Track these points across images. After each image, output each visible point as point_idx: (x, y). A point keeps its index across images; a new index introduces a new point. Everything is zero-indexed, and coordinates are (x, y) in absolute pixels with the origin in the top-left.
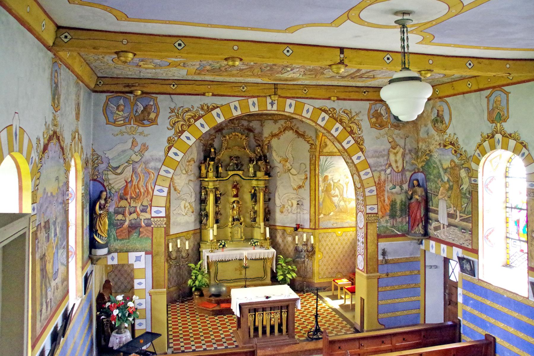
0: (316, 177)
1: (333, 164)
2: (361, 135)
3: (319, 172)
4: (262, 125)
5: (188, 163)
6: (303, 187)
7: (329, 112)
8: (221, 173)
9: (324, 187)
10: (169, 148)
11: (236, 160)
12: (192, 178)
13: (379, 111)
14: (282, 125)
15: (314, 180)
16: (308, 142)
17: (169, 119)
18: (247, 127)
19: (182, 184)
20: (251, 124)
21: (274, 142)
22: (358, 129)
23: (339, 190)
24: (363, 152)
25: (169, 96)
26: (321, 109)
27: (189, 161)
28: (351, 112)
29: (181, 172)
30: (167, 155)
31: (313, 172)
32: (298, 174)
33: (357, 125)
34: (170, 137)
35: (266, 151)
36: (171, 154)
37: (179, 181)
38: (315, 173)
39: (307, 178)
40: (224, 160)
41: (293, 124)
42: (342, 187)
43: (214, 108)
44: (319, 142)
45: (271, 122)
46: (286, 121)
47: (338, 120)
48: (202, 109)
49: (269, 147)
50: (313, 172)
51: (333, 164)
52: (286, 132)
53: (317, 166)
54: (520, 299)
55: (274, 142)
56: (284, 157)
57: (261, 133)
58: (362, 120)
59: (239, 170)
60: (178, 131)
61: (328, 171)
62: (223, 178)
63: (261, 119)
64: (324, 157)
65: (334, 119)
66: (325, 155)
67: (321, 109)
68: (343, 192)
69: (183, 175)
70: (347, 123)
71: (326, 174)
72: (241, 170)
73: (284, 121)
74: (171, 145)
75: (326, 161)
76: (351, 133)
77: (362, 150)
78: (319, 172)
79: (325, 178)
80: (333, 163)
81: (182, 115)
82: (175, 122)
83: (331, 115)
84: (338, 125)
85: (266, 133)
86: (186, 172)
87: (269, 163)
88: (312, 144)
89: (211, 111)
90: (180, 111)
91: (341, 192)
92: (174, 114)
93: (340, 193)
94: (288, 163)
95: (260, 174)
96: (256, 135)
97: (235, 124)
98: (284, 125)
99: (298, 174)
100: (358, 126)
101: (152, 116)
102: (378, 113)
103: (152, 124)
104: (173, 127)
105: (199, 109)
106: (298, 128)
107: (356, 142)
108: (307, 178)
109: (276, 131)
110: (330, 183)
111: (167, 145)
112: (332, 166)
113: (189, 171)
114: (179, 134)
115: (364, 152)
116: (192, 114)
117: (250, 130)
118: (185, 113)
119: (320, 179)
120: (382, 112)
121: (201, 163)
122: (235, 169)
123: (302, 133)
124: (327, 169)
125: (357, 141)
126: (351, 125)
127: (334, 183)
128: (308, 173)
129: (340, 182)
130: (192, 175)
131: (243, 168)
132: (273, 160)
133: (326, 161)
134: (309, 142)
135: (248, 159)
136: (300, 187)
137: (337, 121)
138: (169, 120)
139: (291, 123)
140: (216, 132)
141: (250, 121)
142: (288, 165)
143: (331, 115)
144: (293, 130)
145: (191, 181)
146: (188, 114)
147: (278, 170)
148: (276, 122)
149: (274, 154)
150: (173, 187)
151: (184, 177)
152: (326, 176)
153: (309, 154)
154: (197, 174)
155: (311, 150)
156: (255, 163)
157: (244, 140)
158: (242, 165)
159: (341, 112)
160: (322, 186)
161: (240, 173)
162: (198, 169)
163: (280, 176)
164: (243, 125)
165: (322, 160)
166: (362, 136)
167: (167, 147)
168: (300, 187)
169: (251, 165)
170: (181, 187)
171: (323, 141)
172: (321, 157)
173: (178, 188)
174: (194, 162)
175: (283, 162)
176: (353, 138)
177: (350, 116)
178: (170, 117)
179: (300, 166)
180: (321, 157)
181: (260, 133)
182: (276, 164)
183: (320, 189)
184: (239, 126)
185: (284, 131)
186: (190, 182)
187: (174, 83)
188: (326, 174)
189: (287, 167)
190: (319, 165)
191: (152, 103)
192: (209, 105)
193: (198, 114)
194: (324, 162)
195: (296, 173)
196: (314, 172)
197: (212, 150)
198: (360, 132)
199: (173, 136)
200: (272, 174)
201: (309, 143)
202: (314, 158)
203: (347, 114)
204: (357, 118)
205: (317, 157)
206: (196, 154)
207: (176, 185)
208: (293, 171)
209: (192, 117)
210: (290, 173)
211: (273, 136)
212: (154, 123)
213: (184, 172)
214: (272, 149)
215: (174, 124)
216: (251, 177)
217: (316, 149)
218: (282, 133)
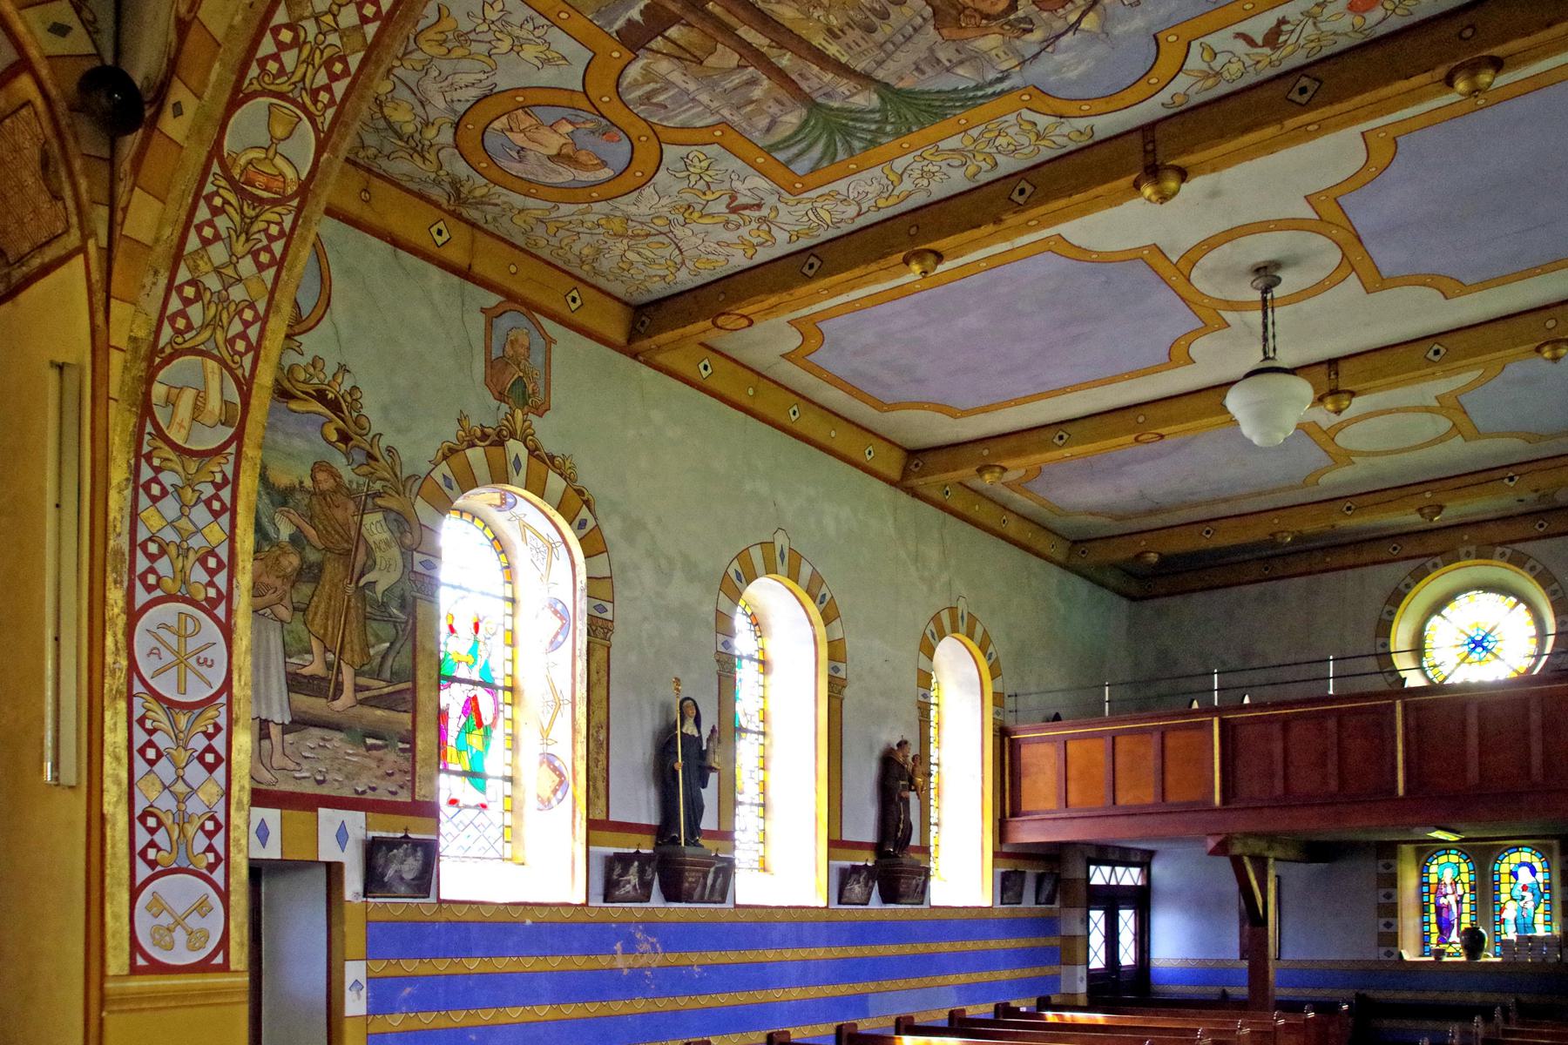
54: (567, 914)
187: (1511, 474)
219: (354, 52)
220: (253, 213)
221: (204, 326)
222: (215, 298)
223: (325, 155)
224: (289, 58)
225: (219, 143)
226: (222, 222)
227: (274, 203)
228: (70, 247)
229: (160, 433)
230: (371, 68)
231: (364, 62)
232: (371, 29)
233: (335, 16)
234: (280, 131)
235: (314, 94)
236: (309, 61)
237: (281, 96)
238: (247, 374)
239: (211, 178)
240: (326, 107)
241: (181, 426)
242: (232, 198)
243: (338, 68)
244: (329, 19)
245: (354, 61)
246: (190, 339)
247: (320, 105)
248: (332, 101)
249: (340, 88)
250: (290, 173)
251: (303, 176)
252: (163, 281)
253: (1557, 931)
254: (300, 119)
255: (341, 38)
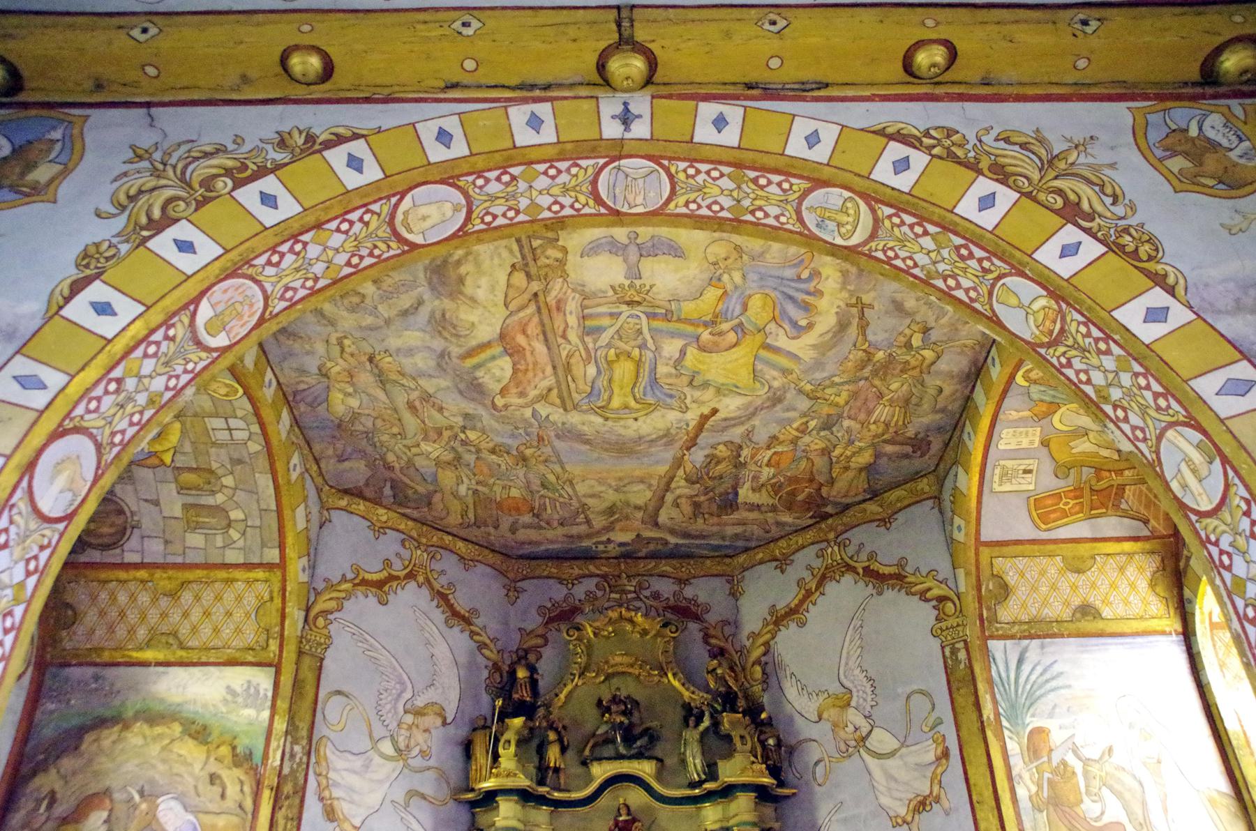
0: (989, 734)
1: (1060, 674)
2: (1133, 221)
3: (997, 714)
4: (735, 595)
5: (409, 719)
6: (937, 800)
7: (927, 141)
8: (557, 770)
9: (1040, 786)
10: (77, 287)
11: (624, 713)
12: (428, 784)
13: (1194, 132)
14: (809, 568)
15: (982, 751)
16: (923, 596)
17: (115, 180)
18: (672, 602)
19: (374, 799)
20: (689, 592)
21: (788, 642)
22: (1109, 201)
23: (1118, 795)
24: (1171, 291)
25: (143, 111)
26: (881, 133)
27: (419, 713)
28: (1042, 141)
29: (367, 744)
30: (54, 312)
31: (969, 717)
32: (903, 745)
33: (1089, 182)
34: (97, 245)
35: (757, 689)
36: (78, 310)
37: (353, 780)
38: (981, 715)
39: (946, 754)
40: (577, 723)
41: (851, 550)
42: (1136, 785)
43: (340, 140)
44: (967, 574)
45: (768, 570)
46: (824, 545)
47: (984, 164)
48: (282, 144)
49: (770, 670)
50: (969, 717)
51: (1060, 674)
52: (830, 587)
53: (981, 687)
55: (788, 642)
56: (835, 688)
57: (733, 623)
58: (1112, 166)
59: (639, 756)
60: (144, 220)
61: (1043, 705)
62: (568, 791)
63: (728, 570)
64: (1009, 642)
65: (960, 163)
66: (1012, 637)
67: (881, 133)
68: (1144, 804)
69: (377, 760)
70: (1036, 176)
71: (1033, 722)
72: (649, 758)
73: (816, 547)
74: (88, 272)
75: (1020, 661)
76: (1071, 212)
77: (1159, 280)
78: (997, 714)
79: (1036, 743)
80: (1057, 668)
81: (180, 166)
82: (140, 192)
83: (936, 151)
84: (984, 185)
85: (753, 615)
86: (398, 750)
87: (769, 722)
88: (942, 599)
89: (320, 151)
90: (176, 156)
91: (1138, 810)
92: (145, 164)
93: (1129, 813)
94: (851, 711)
95: (732, 770)
96: (712, 632)
97: (624, 592)
98: (817, 563)
99: (903, 745)
100: (1102, 186)
101: (42, 173)
102: (1193, 139)
103: (27, 199)
104: (124, 208)
105: (269, 147)
106: (872, 556)
107: (1114, 248)
108: (946, 754)
109: (789, 597)
110: (1064, 763)
111: (73, 273)
112: (1053, 684)
113: (415, 751)
114: (145, 233)
115: (1180, 290)
116: (230, 163)
117: (685, 612)
118: (197, 159)
119: (1012, 746)
120: (1211, 134)
121: (474, 730)
122: (622, 750)
123: (893, 570)
124: (1032, 700)
125: (1122, 247)
126: (1057, 183)
127: (1086, 762)
128: (949, 730)
129: (1117, 758)
130: (431, 775)
131: (658, 752)
132: (791, 720)
133: (1020, 661)
134: (929, 595)
135: (679, 714)
136: (922, 805)
137: (980, 172)
138: (117, 184)
139: (843, 545)
140: (551, 620)
141: (683, 582)
142: (854, 717)
143: (936, 151)
144: (852, 569)
145: (423, 797)
146: (214, 162)
147: (814, 752)
148: (782, 563)
149: (791, 691)
150: (321, 799)
151: (384, 769)
152: (1038, 734)
153: (935, 644)
154: (455, 778)
155: (943, 625)
156: (706, 722)
157: (656, 636)
158: (652, 737)
159: (988, 139)
160: (1026, 776)
161: (645, 769)
162: (458, 752)
163: (826, 776)
164: (656, 596)
165: (999, 656)
166: (1142, 225)
167: (69, 281)
168: (922, 805)
169: (692, 735)
170: (363, 813)
171: (986, 573)
172: (996, 646)
173: (343, 808)
174: (444, 723)
175: (830, 714)
176: (1087, 231)
177: (1043, 152)
178: (125, 174)
179: (908, 712)
180: (996, 646)
181: (726, 623)
182: (805, 729)
183: (1021, 792)
184: (638, 598)
185: (820, 584)
186: (415, 801)
188: (1033, 722)
189: (850, 728)
190: (990, 682)
191: (57, 135)
192: (316, 131)
193: (259, 160)
194: (1013, 666)
195: (896, 745)
196: (974, 716)
197: (522, 673)
198: (1119, 210)
199: (114, 241)
200: (789, 776)
201: (927, 600)
202: (962, 655)
203: (1023, 146)
204: (1082, 159)
205: (975, 643)
206: (454, 695)
207: (336, 793)
208: (882, 740)
209: (228, 172)
210: (869, 751)
211: (779, 619)
212: (44, 198)
213: (387, 747)
214: (781, 674)
215: (132, 199)
216: (693, 785)
217: (960, 612)
218: (813, 598)
219: (950, 240)
220: (1071, 339)
221: (1144, 420)
222: (1128, 398)
223: (1028, 272)
224: (966, 283)
225: (1027, 343)
226: (1077, 364)
227: (1063, 319)
228: (289, 604)
229: (1197, 513)
230: (959, 229)
231: (956, 233)
232: (932, 229)
233: (929, 252)
234: (1014, 301)
235: (985, 271)
236: (965, 270)
237: (990, 294)
238: (1184, 413)
239: (1048, 357)
240: (993, 264)
241: (1200, 495)
242: (1061, 349)
243: (964, 252)
244: (933, 255)
245: (958, 241)
246: (1152, 433)
247: (993, 268)
248: (988, 259)
249: (979, 253)
250: (1043, 302)
251: (1045, 293)
252: (1111, 425)
253: (709, 828)
254: (1004, 284)
255: (943, 248)
